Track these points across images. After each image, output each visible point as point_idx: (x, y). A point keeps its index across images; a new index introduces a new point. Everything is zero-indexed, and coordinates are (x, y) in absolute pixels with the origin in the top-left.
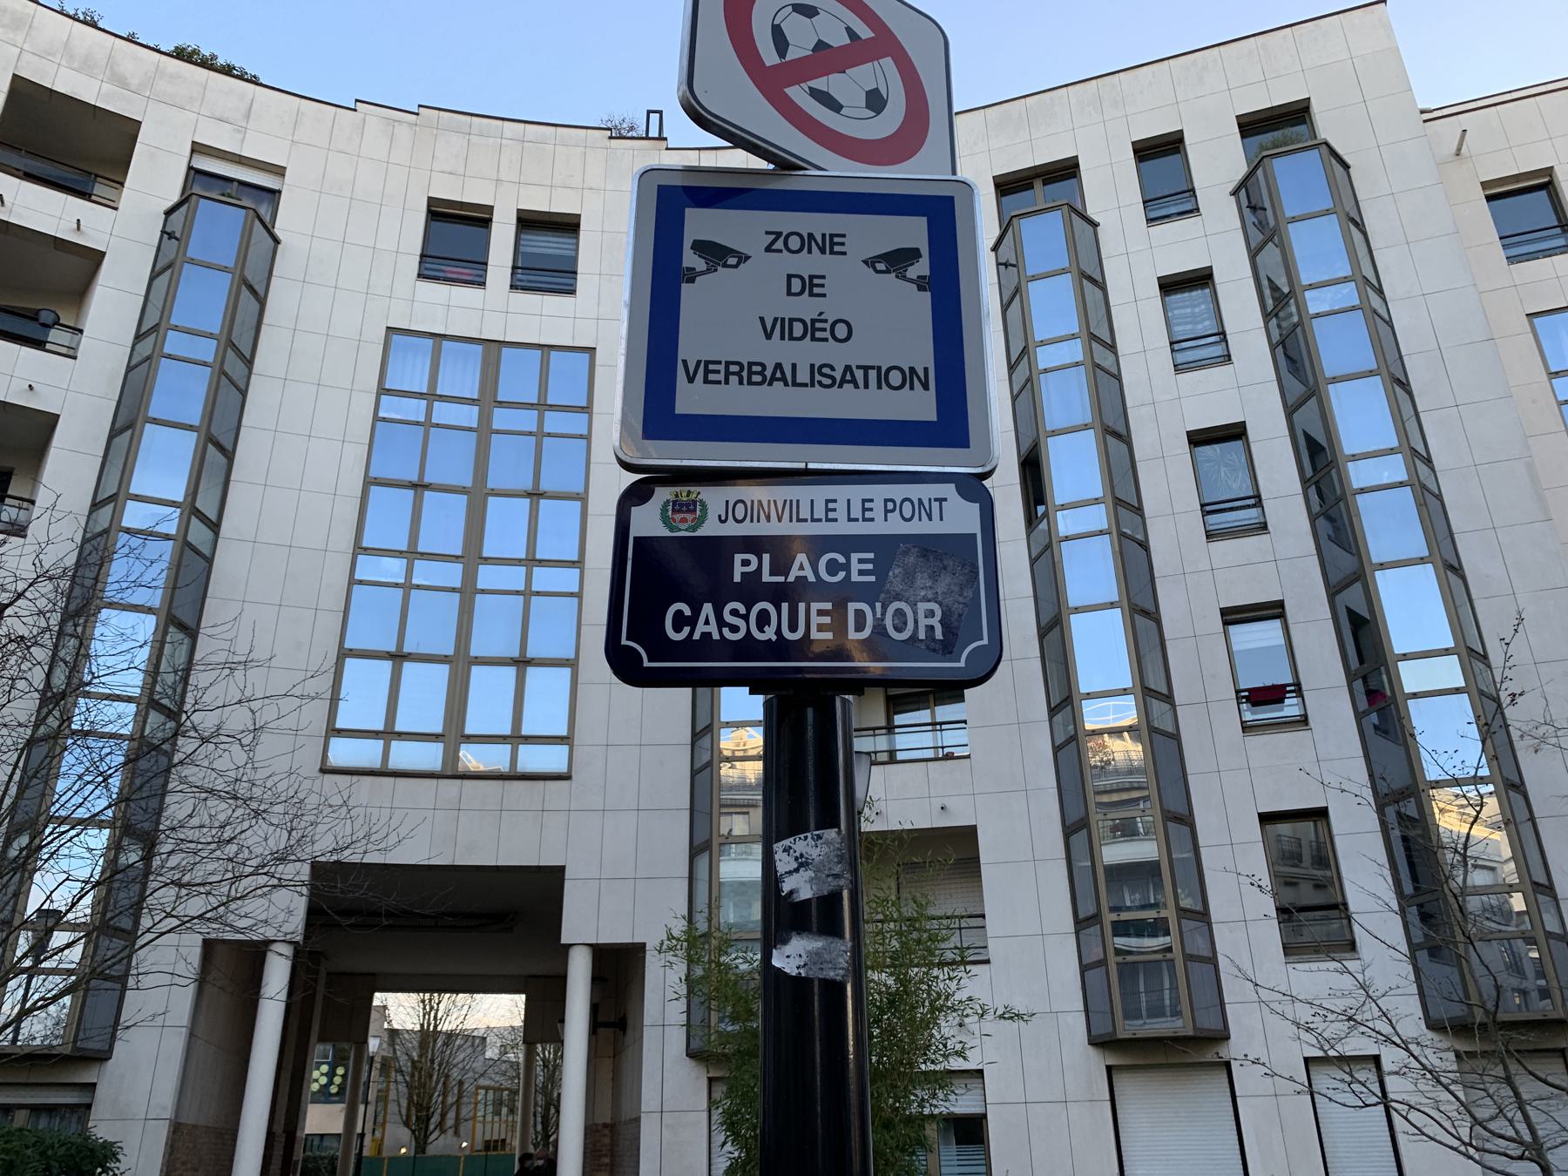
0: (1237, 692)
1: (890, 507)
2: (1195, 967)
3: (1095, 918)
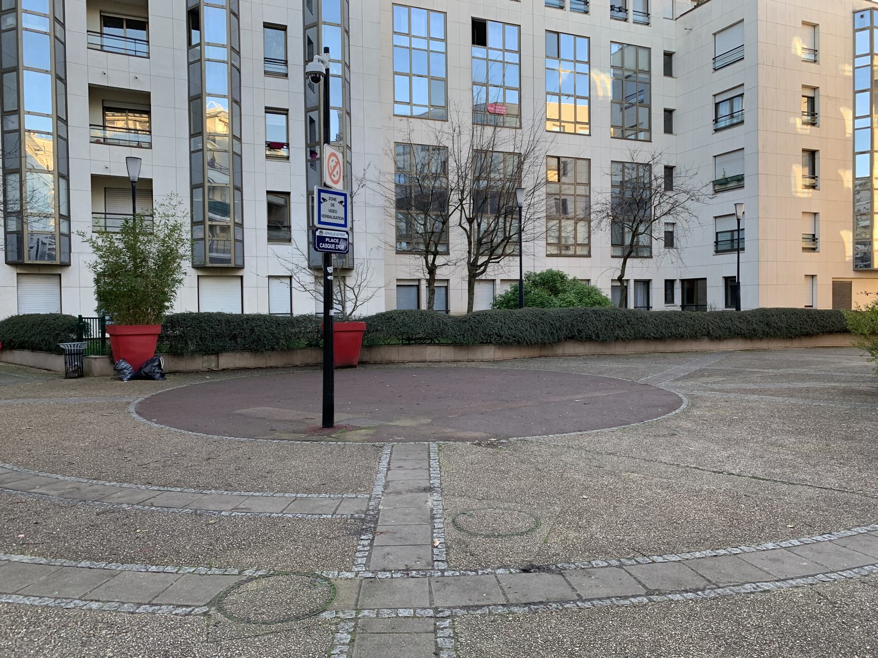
0: (266, 142)
1: (340, 234)
2: (237, 243)
3: (202, 223)
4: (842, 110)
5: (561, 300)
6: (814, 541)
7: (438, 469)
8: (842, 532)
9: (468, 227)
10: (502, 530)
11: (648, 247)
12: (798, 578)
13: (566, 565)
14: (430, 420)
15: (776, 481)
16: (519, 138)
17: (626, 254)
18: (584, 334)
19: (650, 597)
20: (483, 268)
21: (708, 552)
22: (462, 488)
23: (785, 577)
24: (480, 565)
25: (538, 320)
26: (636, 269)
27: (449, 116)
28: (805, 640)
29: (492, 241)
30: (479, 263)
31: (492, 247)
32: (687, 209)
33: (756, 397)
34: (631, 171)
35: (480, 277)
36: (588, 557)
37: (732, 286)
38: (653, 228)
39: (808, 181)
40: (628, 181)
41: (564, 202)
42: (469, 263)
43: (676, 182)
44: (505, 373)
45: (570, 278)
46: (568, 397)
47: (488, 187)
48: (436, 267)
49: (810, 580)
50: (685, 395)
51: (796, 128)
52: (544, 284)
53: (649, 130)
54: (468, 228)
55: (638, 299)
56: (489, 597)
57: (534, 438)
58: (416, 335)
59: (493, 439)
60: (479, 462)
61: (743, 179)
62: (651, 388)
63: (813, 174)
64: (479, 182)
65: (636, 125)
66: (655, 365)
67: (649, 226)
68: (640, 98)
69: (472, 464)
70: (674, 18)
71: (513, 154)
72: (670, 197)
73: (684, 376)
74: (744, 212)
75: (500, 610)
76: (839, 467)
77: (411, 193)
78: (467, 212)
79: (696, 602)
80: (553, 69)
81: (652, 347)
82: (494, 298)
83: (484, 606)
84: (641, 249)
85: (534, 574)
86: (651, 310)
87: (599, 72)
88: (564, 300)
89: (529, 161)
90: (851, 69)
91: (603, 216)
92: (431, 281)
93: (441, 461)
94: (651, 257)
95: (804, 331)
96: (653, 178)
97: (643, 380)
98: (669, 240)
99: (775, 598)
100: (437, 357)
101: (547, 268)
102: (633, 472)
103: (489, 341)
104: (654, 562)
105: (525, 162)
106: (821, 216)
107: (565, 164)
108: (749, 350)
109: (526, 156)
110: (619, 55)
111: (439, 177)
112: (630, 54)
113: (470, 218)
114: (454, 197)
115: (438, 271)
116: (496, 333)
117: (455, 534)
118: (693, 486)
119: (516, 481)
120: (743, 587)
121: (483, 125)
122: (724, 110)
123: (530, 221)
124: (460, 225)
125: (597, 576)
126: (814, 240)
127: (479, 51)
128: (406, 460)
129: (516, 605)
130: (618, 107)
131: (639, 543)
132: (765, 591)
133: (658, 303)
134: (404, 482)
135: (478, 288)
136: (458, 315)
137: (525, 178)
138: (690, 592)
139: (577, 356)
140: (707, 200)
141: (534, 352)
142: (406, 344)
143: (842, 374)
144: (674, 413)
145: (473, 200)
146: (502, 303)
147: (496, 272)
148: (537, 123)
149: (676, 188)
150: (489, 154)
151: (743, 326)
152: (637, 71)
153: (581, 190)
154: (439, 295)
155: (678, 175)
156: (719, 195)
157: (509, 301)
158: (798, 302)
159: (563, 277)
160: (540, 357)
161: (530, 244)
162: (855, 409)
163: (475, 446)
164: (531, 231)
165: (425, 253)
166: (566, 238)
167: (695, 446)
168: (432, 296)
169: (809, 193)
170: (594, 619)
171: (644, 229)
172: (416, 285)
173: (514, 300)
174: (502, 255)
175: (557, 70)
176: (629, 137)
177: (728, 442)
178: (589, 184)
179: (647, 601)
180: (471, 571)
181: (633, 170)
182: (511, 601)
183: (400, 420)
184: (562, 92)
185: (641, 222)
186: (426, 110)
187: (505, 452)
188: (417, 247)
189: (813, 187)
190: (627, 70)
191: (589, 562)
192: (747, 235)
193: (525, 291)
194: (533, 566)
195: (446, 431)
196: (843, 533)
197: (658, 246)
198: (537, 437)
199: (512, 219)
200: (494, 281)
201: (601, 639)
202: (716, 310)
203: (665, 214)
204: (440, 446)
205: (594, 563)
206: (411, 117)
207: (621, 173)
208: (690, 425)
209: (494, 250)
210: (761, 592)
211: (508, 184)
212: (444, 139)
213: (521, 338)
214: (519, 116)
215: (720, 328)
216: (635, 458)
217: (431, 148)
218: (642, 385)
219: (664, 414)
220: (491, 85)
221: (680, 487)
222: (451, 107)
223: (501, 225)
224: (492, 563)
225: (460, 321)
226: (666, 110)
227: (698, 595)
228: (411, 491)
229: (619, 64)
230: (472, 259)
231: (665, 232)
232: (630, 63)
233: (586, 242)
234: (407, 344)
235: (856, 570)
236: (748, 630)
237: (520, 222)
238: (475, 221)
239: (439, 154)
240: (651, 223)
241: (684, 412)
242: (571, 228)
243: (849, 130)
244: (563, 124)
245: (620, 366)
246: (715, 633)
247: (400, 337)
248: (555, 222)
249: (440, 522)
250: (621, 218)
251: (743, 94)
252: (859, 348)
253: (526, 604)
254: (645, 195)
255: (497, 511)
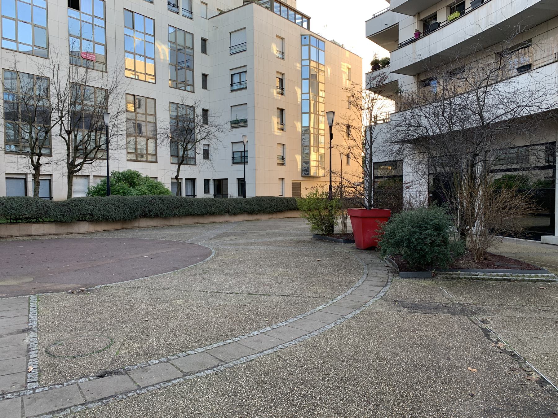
4: (296, 88)
5: (137, 190)
6: (278, 327)
7: (37, 314)
8: (292, 319)
9: (67, 137)
10: (86, 351)
11: (193, 158)
12: (268, 349)
13: (131, 367)
14: (32, 279)
15: (260, 295)
16: (105, 78)
17: (180, 162)
18: (152, 213)
19: (185, 377)
20: (79, 167)
21: (221, 343)
22: (55, 325)
23: (262, 350)
24: (66, 379)
25: (120, 204)
26: (186, 172)
27: (50, 56)
28: (271, 384)
29: (86, 148)
30: (76, 163)
31: (86, 152)
32: (216, 137)
33: (252, 247)
34: (182, 110)
35: (77, 173)
36: (147, 359)
37: (242, 183)
38: (196, 147)
39: (280, 126)
40: (180, 116)
41: (139, 125)
42: (68, 163)
43: (210, 119)
44: (96, 241)
45: (143, 176)
46: (140, 255)
47: (82, 110)
48: (40, 165)
49: (275, 349)
50: (214, 248)
51: (274, 95)
52: (125, 180)
53: (193, 85)
54: (67, 137)
55: (188, 191)
56: (71, 401)
57: (113, 285)
58: (22, 215)
59: (83, 288)
60: (72, 305)
61: (247, 121)
62: (193, 246)
63: (282, 123)
64: (75, 106)
65: (185, 81)
66: (198, 231)
67: (193, 145)
68: (187, 64)
69: (65, 307)
70: (207, 18)
71: (101, 89)
72: (206, 129)
73: (214, 237)
74: (247, 141)
75: (80, 408)
76: (292, 283)
77: (18, 108)
78: (66, 126)
79: (213, 375)
80: (130, 36)
81: (196, 220)
82: (89, 189)
83: (66, 408)
84: (189, 160)
85: (107, 377)
86: (196, 197)
87: (161, 44)
88: (139, 190)
89: (113, 95)
90: (300, 66)
91: (165, 137)
92: (36, 176)
93: (39, 308)
94: (195, 165)
95: (278, 209)
96: (196, 116)
97: (189, 241)
98: (206, 154)
99: (256, 364)
100: (41, 232)
101: (128, 169)
102: (179, 299)
103: (84, 219)
104: (188, 355)
105: (110, 95)
106: (286, 146)
107: (140, 101)
108: (250, 220)
109: (111, 92)
110: (174, 34)
111: (42, 99)
112: (180, 35)
113: (68, 131)
114: (55, 115)
115: (42, 168)
116: (89, 213)
117: (47, 360)
118: (215, 303)
119: (98, 315)
120: (240, 360)
121: (77, 66)
122: (236, 79)
123: (114, 136)
124: (60, 135)
125: (151, 371)
126: (283, 159)
127: (73, 12)
128: (8, 311)
129: (92, 402)
130: (174, 68)
131: (180, 344)
132: (251, 360)
133: (200, 193)
134: (5, 327)
135: (76, 181)
136: (60, 200)
137: (110, 107)
138: (209, 369)
139: (148, 227)
140: (227, 132)
141: (118, 226)
142: (14, 223)
143: (296, 232)
144: (206, 260)
145: (71, 118)
146: (95, 192)
147: (90, 170)
148: (118, 70)
149: (209, 123)
150: (83, 87)
151: (247, 207)
152: (185, 47)
153: (150, 119)
154: (43, 187)
155: (210, 115)
156: (234, 130)
157: (99, 191)
158: (275, 193)
159: (138, 175)
160: (122, 229)
161: (116, 152)
162: (301, 250)
163: (68, 294)
164: (115, 143)
165: (31, 154)
166: (141, 149)
167: (218, 279)
168: (37, 187)
169: (280, 133)
170: (148, 400)
171: (191, 147)
172: (24, 178)
173: (103, 190)
174: (94, 158)
175: (132, 37)
176: (181, 88)
177: (236, 275)
178: (155, 115)
179: (183, 380)
180: (58, 384)
181: (183, 109)
182: (88, 400)
183: (5, 281)
184: (136, 53)
185: (189, 142)
186: (30, 48)
187: (91, 296)
188: (23, 150)
189: (283, 129)
190: (178, 45)
191: (147, 362)
192: (250, 155)
193: (111, 184)
194: (106, 372)
195: (46, 286)
196: (292, 319)
197: (200, 158)
198: (116, 283)
199: (101, 133)
200: (88, 176)
201: (152, 412)
202: (233, 197)
203: (203, 139)
204: (39, 297)
205: (150, 362)
206: (16, 51)
207: (176, 110)
208: (215, 266)
209: (88, 155)
210: (249, 361)
211: (98, 109)
212: (46, 72)
213: (108, 216)
214: (106, 64)
215: (235, 208)
216: (181, 290)
217: (35, 77)
218: (189, 244)
219: (201, 261)
220: (83, 39)
221: (207, 305)
222: (51, 50)
223: (93, 137)
224: (75, 376)
225: (61, 205)
226: (203, 74)
227: (214, 370)
228: (11, 334)
229: (174, 41)
230: (71, 160)
231: (204, 150)
232: (180, 41)
233: (154, 153)
234: (15, 223)
235: (297, 340)
236: (241, 386)
237: (107, 136)
238: (73, 133)
239: (41, 82)
240: (195, 144)
241: (212, 259)
242: (144, 143)
243: (299, 100)
244: (137, 74)
245: (176, 233)
246: (222, 391)
247: (8, 218)
248: (132, 138)
249: (35, 353)
250: (176, 139)
251: (246, 71)
252: (303, 218)
253: (99, 400)
254: (191, 125)
255: (82, 338)
